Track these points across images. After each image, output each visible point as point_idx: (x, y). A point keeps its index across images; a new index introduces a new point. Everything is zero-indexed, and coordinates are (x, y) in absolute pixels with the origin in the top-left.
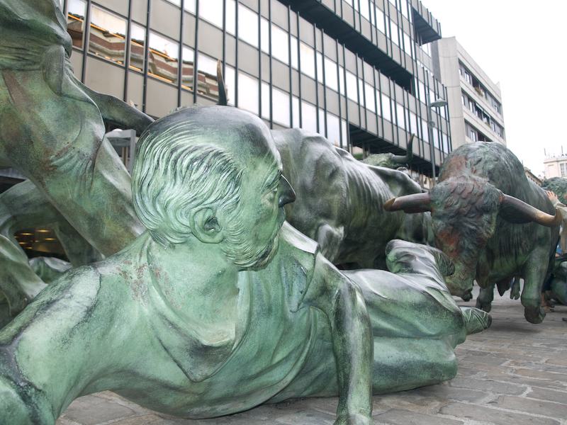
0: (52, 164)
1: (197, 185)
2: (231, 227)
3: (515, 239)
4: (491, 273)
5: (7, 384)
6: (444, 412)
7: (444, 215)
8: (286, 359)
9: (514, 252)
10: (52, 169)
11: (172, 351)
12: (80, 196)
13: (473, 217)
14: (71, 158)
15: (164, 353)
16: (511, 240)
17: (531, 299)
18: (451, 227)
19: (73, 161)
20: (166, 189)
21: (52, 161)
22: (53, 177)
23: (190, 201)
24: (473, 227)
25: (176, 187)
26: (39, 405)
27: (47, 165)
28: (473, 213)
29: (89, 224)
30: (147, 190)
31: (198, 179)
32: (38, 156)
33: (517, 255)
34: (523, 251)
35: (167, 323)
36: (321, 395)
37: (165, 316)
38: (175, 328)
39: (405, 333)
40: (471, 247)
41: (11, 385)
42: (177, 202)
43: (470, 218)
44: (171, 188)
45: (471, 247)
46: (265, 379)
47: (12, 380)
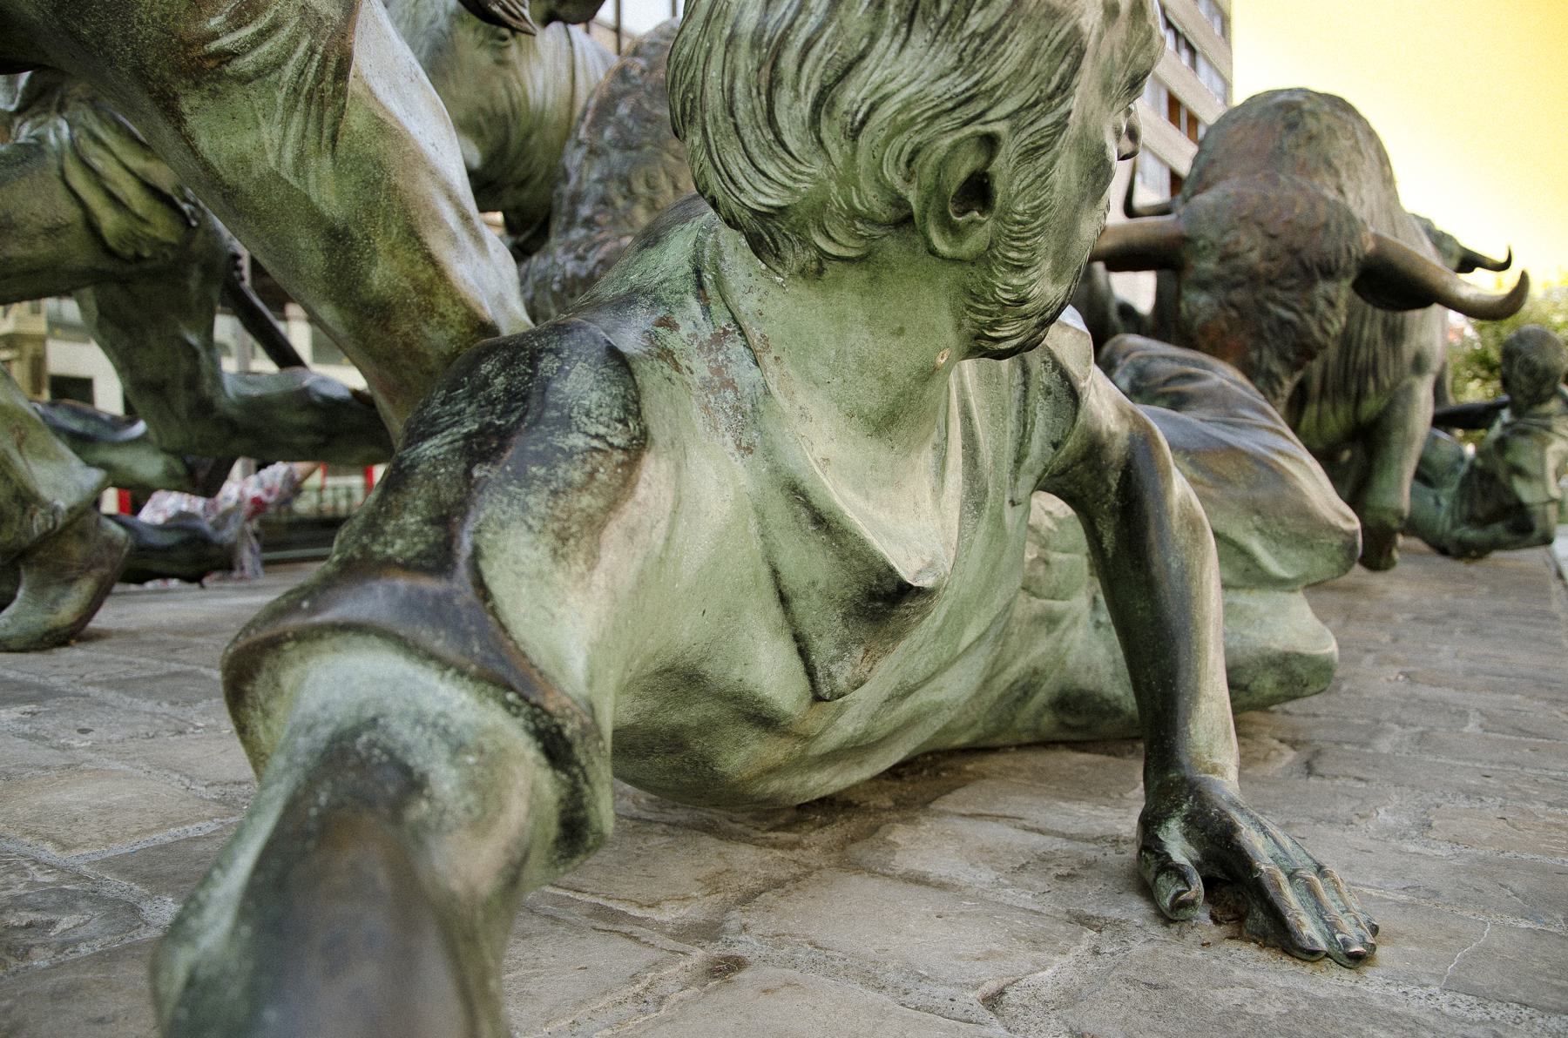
0: (214, 46)
1: (987, 48)
2: (1020, 208)
3: (1363, 352)
5: (491, 702)
6: (1320, 770)
7: (1219, 278)
8: (981, 638)
9: (1353, 388)
10: (212, 63)
11: (799, 605)
12: (301, 158)
13: (1290, 289)
14: (275, 27)
15: (775, 611)
16: (1352, 358)
17: (1385, 510)
18: (1234, 314)
19: (282, 36)
20: (870, 62)
21: (215, 36)
22: (214, 94)
23: (950, 105)
24: (1287, 315)
25: (908, 53)
26: (589, 769)
27: (196, 52)
28: (1292, 275)
29: (330, 251)
30: (800, 67)
31: (992, 30)
32: (164, 17)
33: (1361, 395)
34: (1377, 386)
35: (805, 515)
36: (999, 741)
37: (804, 494)
38: (828, 530)
41: (507, 706)
42: (907, 105)
43: (1281, 289)
44: (891, 55)
46: (924, 697)
47: (510, 688)
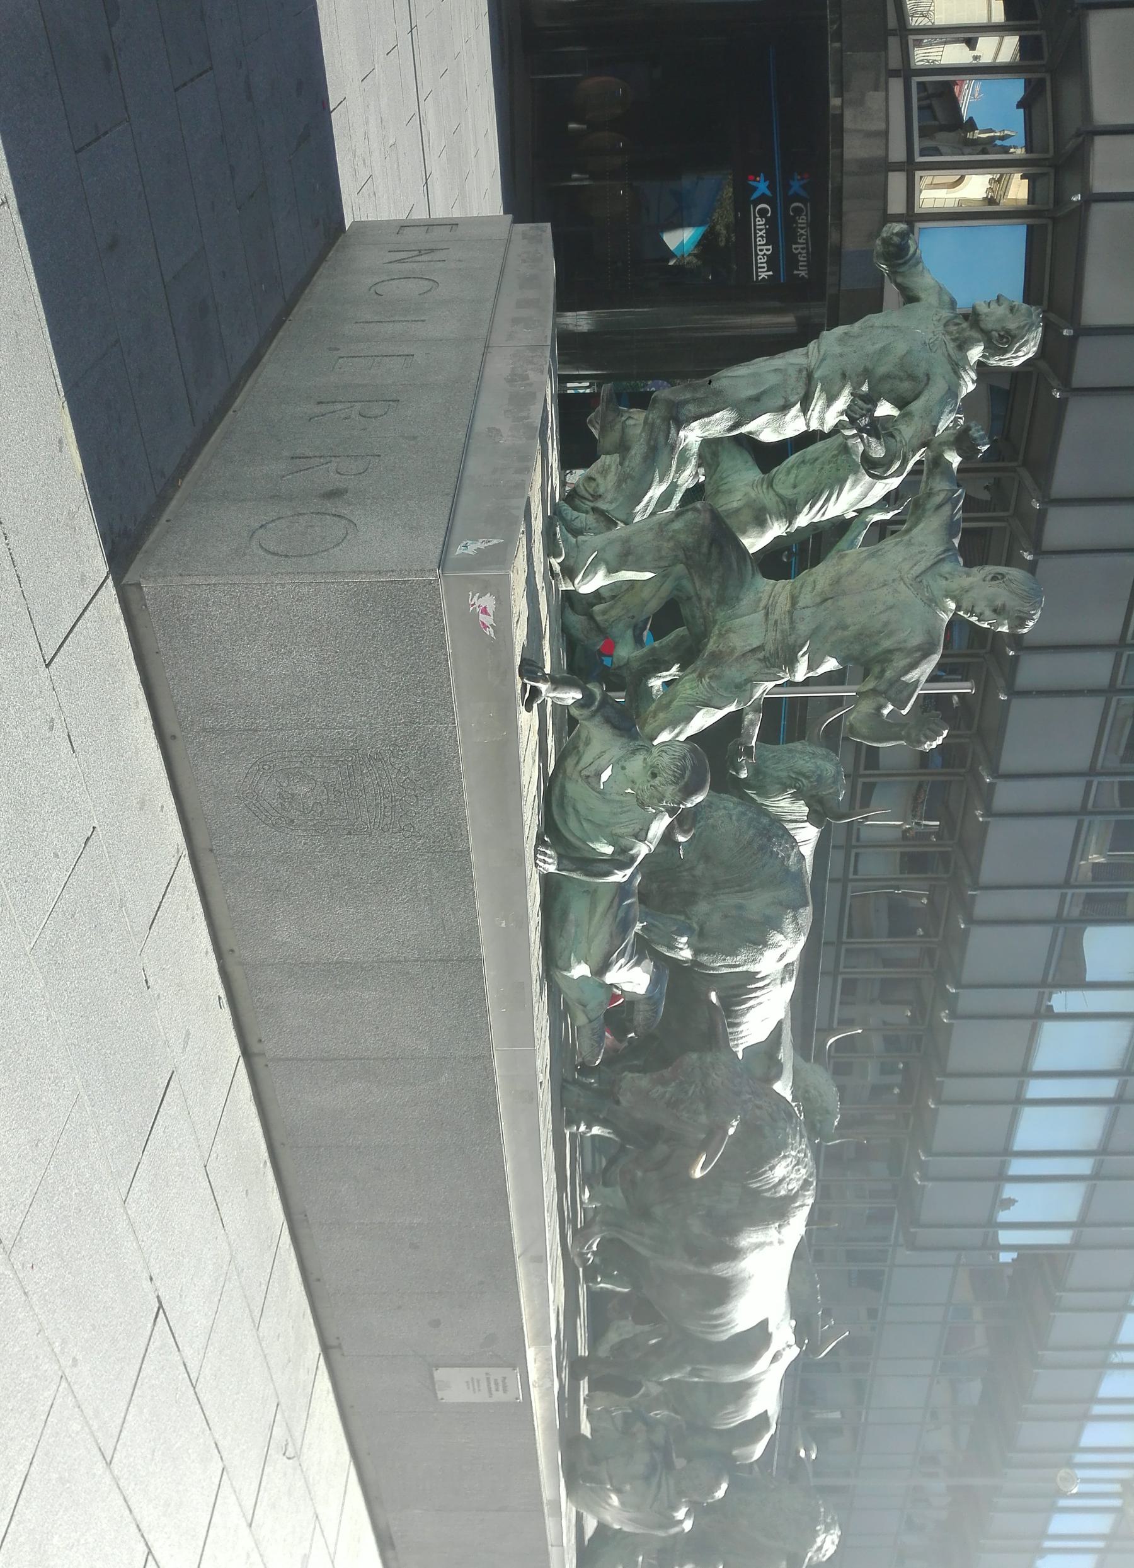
4: (639, 1174)
39: (592, 930)
40: (667, 1095)
45: (667, 1095)
